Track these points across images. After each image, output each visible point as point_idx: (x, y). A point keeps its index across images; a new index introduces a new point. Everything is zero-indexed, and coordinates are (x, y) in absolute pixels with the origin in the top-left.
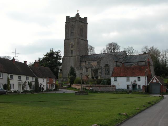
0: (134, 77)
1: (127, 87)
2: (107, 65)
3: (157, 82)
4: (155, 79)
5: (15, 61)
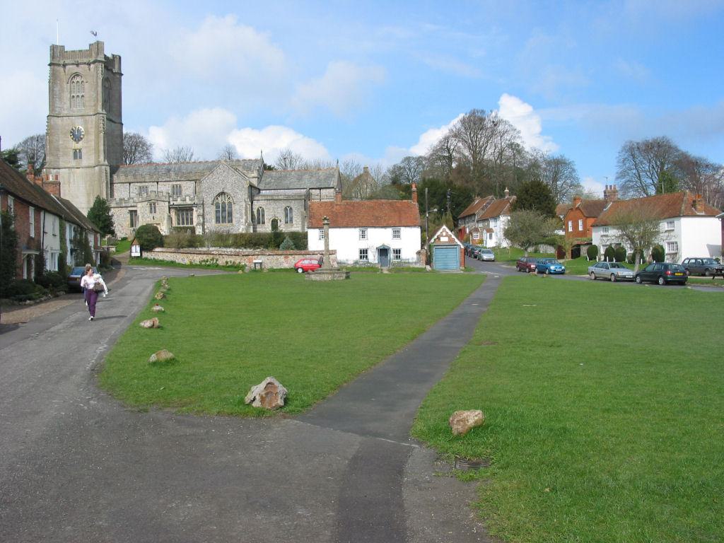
0: (383, 229)
1: (361, 253)
2: (223, 193)
3: (451, 240)
4: (444, 234)
5: (664, 226)
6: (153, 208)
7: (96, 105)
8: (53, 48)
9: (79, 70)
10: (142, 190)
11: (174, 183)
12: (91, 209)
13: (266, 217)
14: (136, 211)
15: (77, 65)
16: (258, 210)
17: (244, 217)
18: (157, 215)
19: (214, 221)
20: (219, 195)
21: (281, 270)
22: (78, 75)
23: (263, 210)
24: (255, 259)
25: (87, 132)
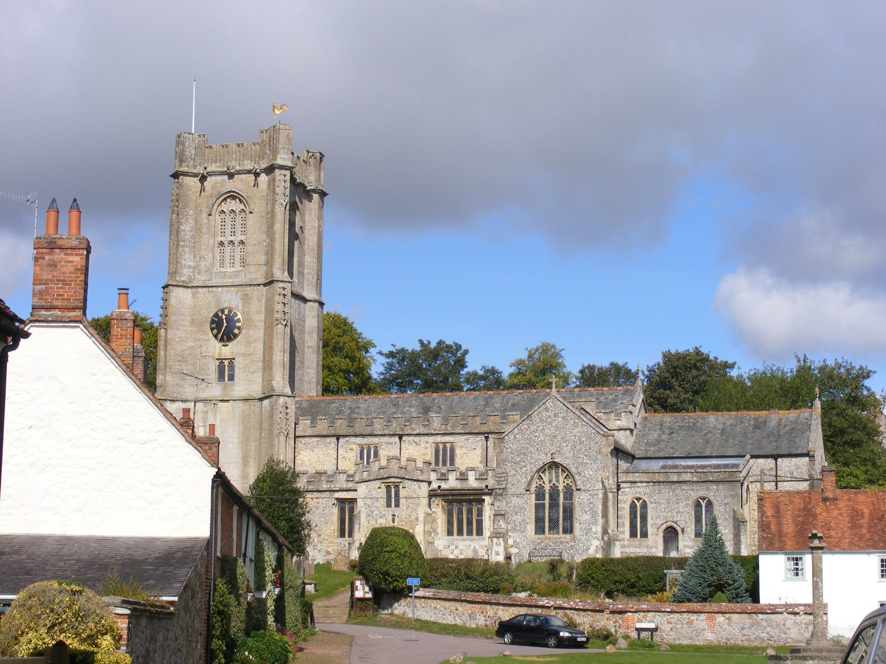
6: (393, 498)
7: (269, 263)
8: (356, 499)
9: (240, 184)
10: (368, 455)
11: (439, 439)
12: (229, 481)
13: (650, 522)
14: (353, 501)
15: (231, 176)
16: (633, 507)
17: (601, 521)
18: (402, 512)
19: (531, 527)
20: (542, 470)
21: (697, 649)
22: (234, 198)
23: (644, 506)
24: (640, 621)
25: (249, 320)
